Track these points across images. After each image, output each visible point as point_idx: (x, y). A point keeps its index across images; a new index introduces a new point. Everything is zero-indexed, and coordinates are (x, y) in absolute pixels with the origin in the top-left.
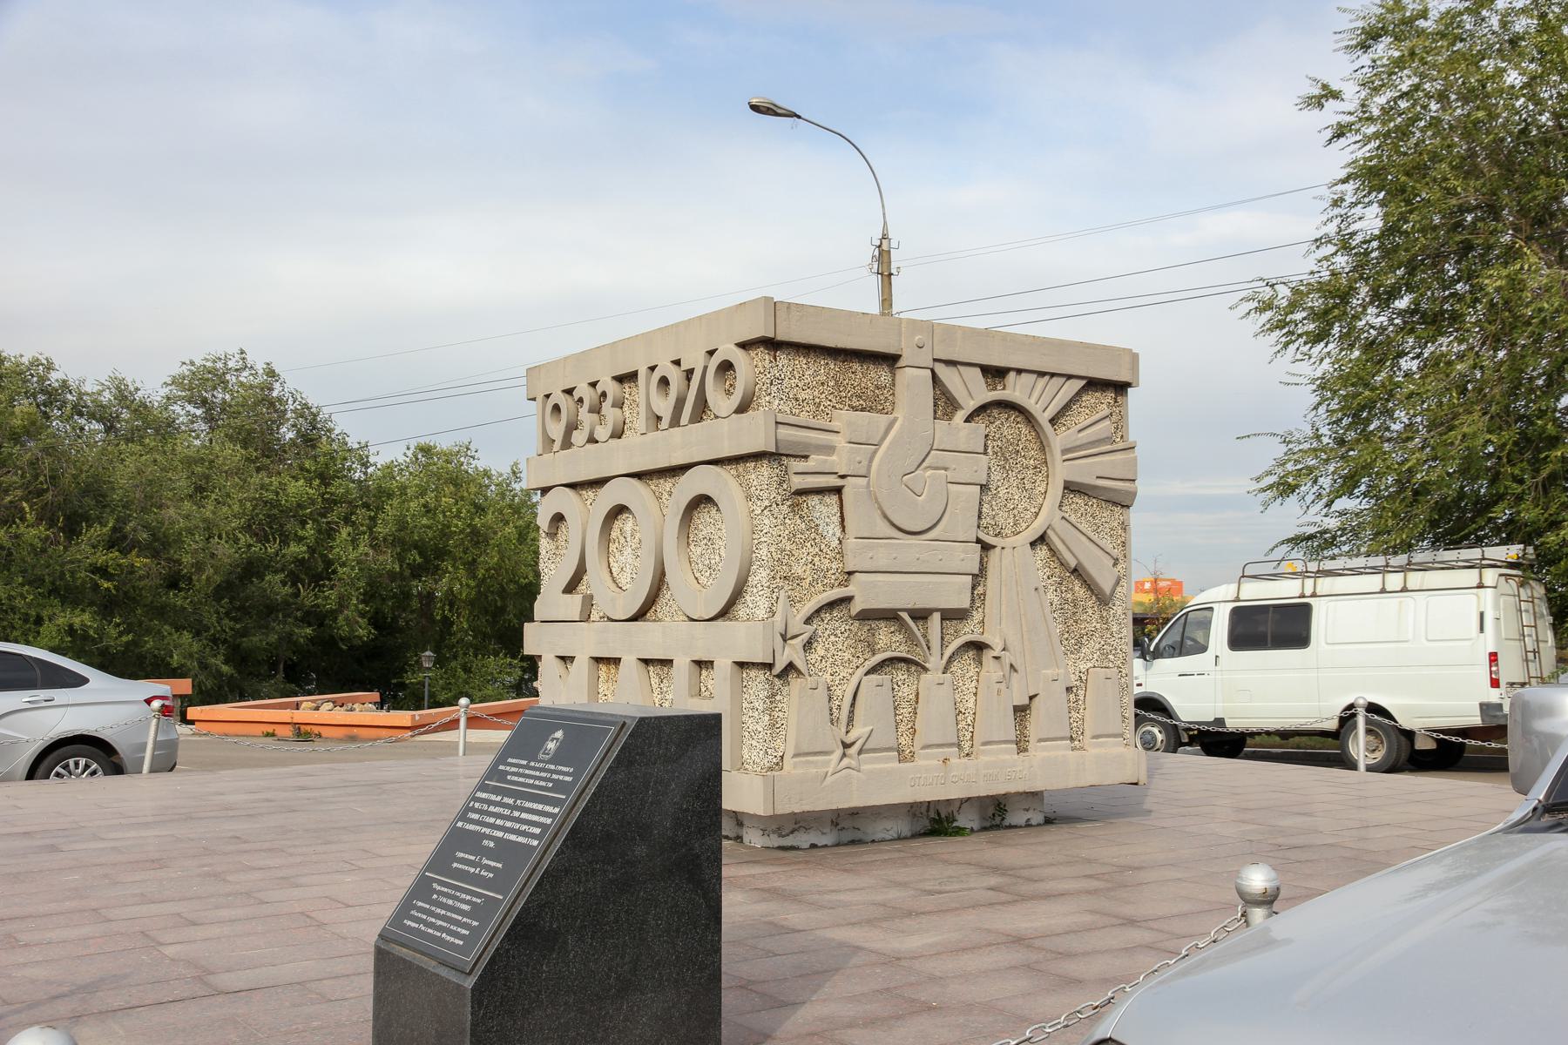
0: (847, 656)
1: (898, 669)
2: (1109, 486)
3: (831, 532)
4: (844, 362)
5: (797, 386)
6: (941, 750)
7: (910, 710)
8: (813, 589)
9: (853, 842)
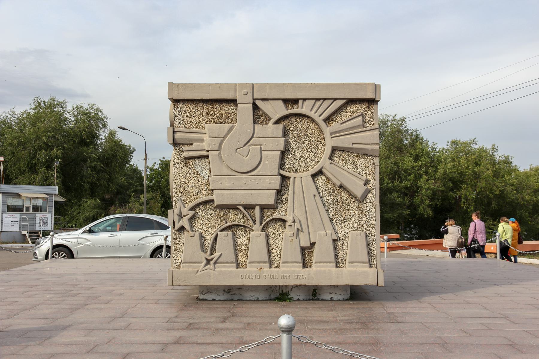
0: (213, 224)
1: (240, 230)
2: (367, 148)
3: (204, 174)
4: (211, 104)
5: (188, 116)
6: (260, 264)
7: (245, 247)
8: (196, 197)
9: (239, 300)
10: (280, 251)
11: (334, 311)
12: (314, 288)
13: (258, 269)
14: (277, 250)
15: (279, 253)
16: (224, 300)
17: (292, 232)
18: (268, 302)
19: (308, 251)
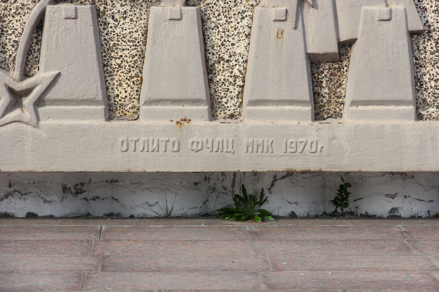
7: (134, 52)
9: (110, 216)
10: (241, 69)
11: (414, 252)
12: (343, 180)
13: (174, 123)
14: (234, 63)
15: (238, 74)
16: (65, 218)
17: (283, 6)
18: (203, 223)
19: (330, 69)
